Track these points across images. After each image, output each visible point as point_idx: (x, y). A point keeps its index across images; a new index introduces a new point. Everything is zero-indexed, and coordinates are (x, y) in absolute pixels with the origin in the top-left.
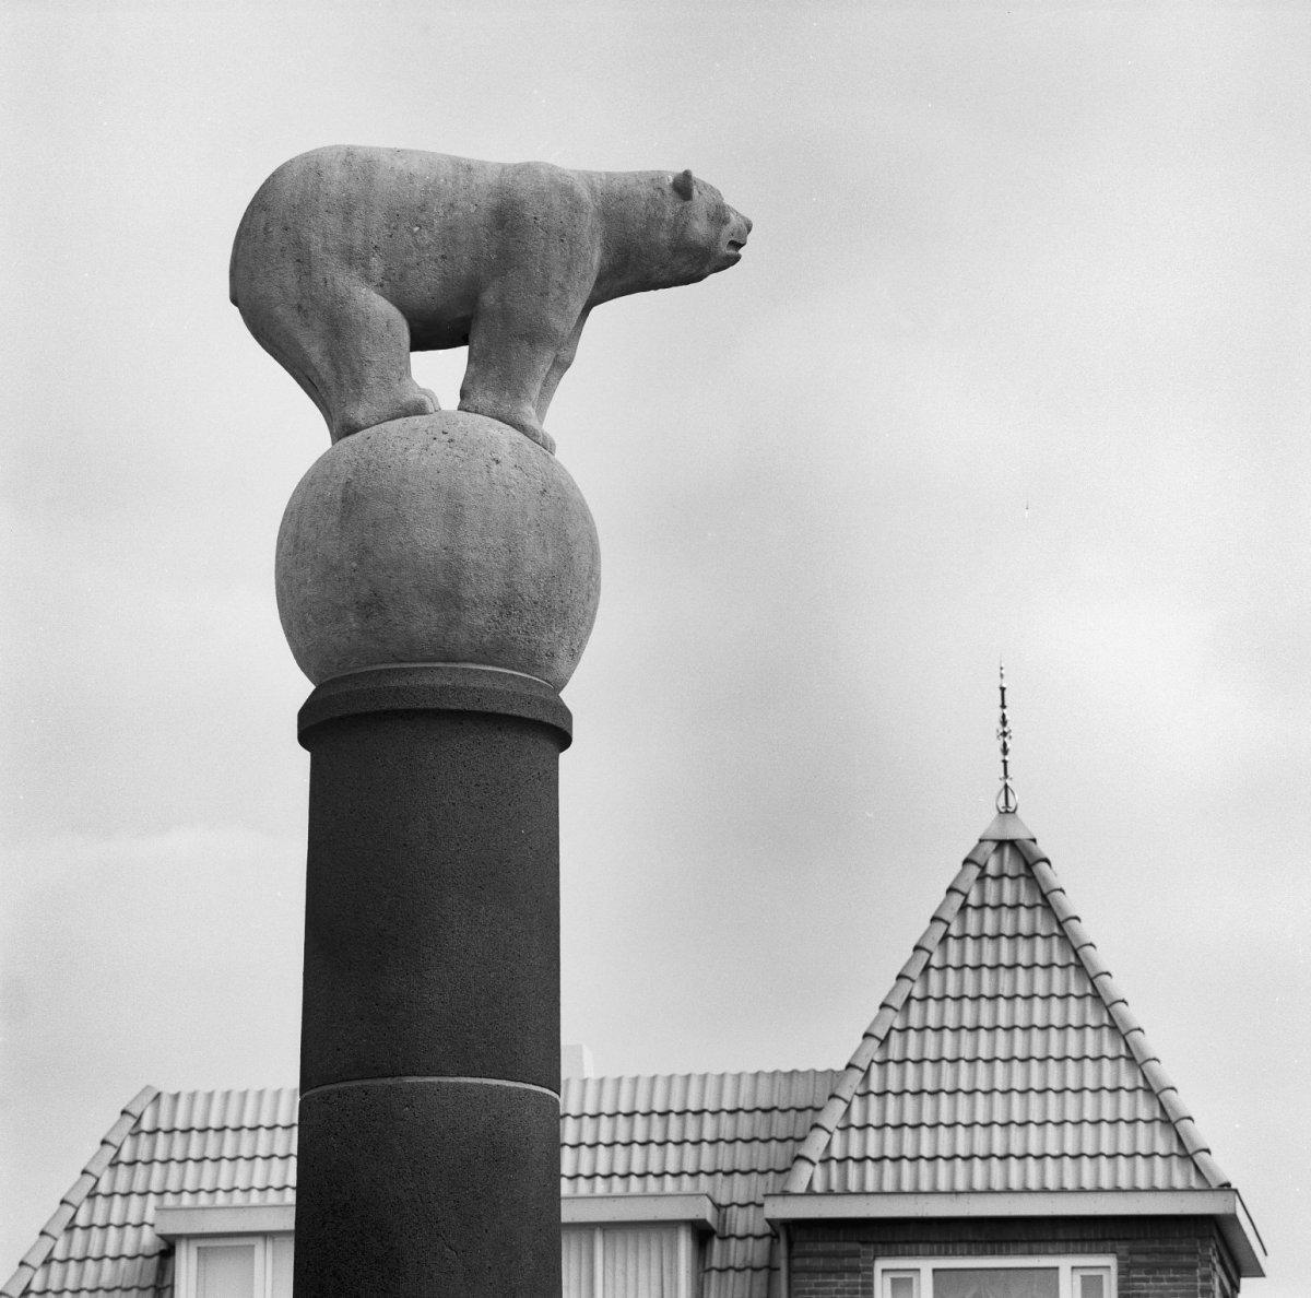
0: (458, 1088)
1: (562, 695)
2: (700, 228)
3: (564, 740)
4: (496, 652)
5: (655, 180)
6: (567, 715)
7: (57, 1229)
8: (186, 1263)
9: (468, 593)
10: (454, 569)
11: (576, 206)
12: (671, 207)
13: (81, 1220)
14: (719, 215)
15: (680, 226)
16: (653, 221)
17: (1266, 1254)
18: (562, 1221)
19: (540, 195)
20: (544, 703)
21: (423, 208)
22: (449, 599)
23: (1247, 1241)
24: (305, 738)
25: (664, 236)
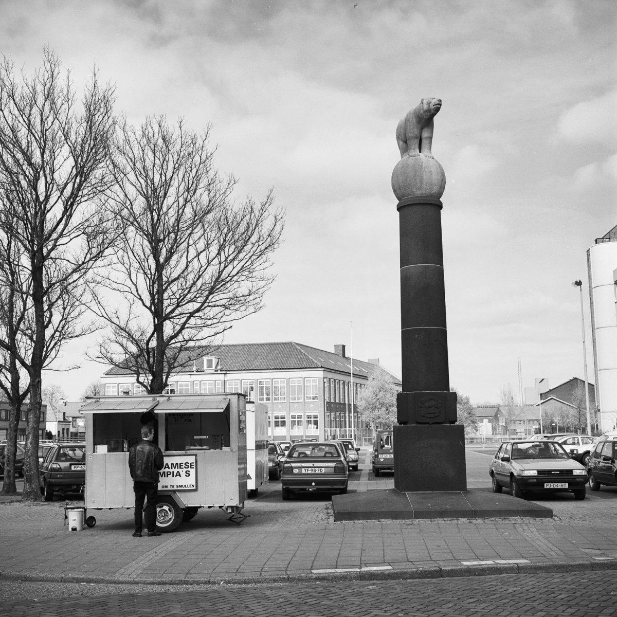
1: (441, 199)
3: (441, 208)
16: (420, 110)
25: (422, 112)
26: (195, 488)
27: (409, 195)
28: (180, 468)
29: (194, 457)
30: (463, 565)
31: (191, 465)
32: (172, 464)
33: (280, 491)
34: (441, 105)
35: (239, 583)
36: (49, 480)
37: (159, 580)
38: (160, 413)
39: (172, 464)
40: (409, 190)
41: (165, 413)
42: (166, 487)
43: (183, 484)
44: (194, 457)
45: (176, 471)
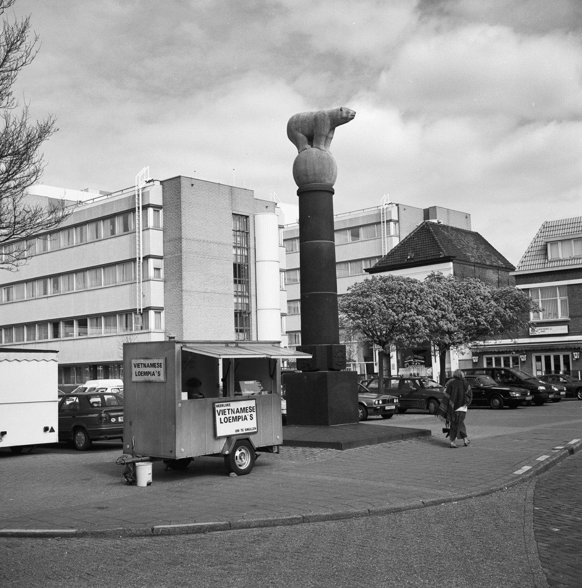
0: (312, 243)
1: (333, 187)
2: (344, 115)
3: (333, 193)
4: (315, 181)
5: (337, 110)
6: (334, 190)
7: (533, 243)
8: (549, 246)
9: (309, 174)
10: (306, 170)
11: (325, 116)
12: (340, 112)
13: (536, 241)
14: (348, 113)
15: (341, 115)
16: (337, 115)
17: (57, 352)
18: (336, 261)
19: (320, 115)
20: (331, 188)
21: (306, 120)
22: (306, 175)
23: (575, 278)
24: (298, 195)
25: (339, 117)
26: (256, 430)
27: (321, 182)
28: (247, 412)
29: (254, 401)
30: (515, 474)
31: (253, 409)
32: (241, 408)
33: (173, 451)
34: (354, 116)
35: (260, 526)
36: (543, 373)
37: (170, 537)
38: (232, 358)
39: (241, 408)
40: (323, 179)
41: (235, 358)
42: (238, 431)
43: (249, 427)
44: (254, 401)
45: (243, 414)
